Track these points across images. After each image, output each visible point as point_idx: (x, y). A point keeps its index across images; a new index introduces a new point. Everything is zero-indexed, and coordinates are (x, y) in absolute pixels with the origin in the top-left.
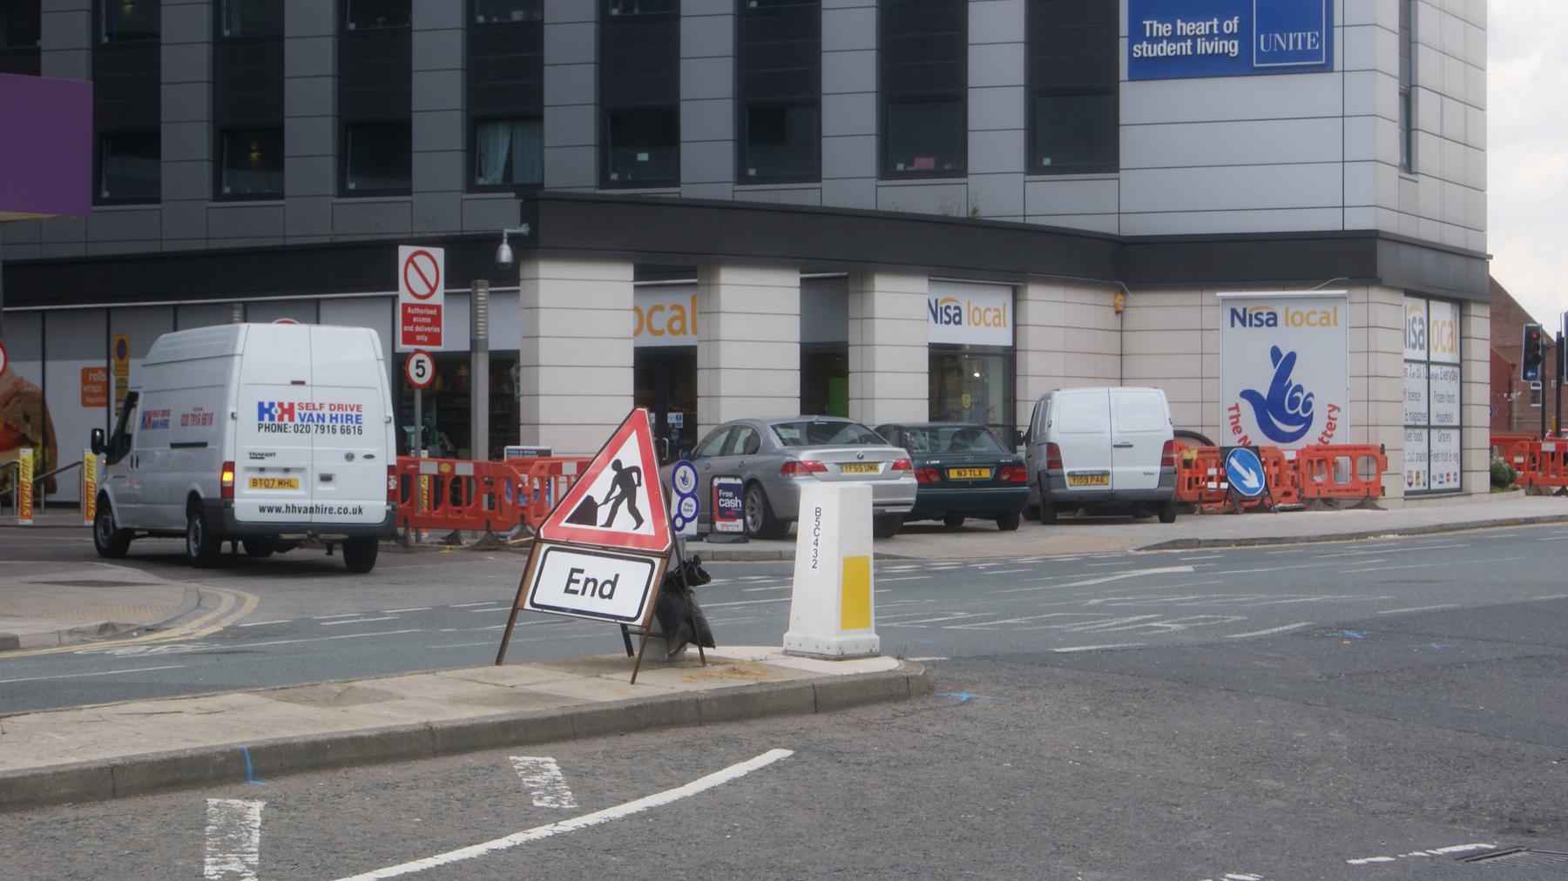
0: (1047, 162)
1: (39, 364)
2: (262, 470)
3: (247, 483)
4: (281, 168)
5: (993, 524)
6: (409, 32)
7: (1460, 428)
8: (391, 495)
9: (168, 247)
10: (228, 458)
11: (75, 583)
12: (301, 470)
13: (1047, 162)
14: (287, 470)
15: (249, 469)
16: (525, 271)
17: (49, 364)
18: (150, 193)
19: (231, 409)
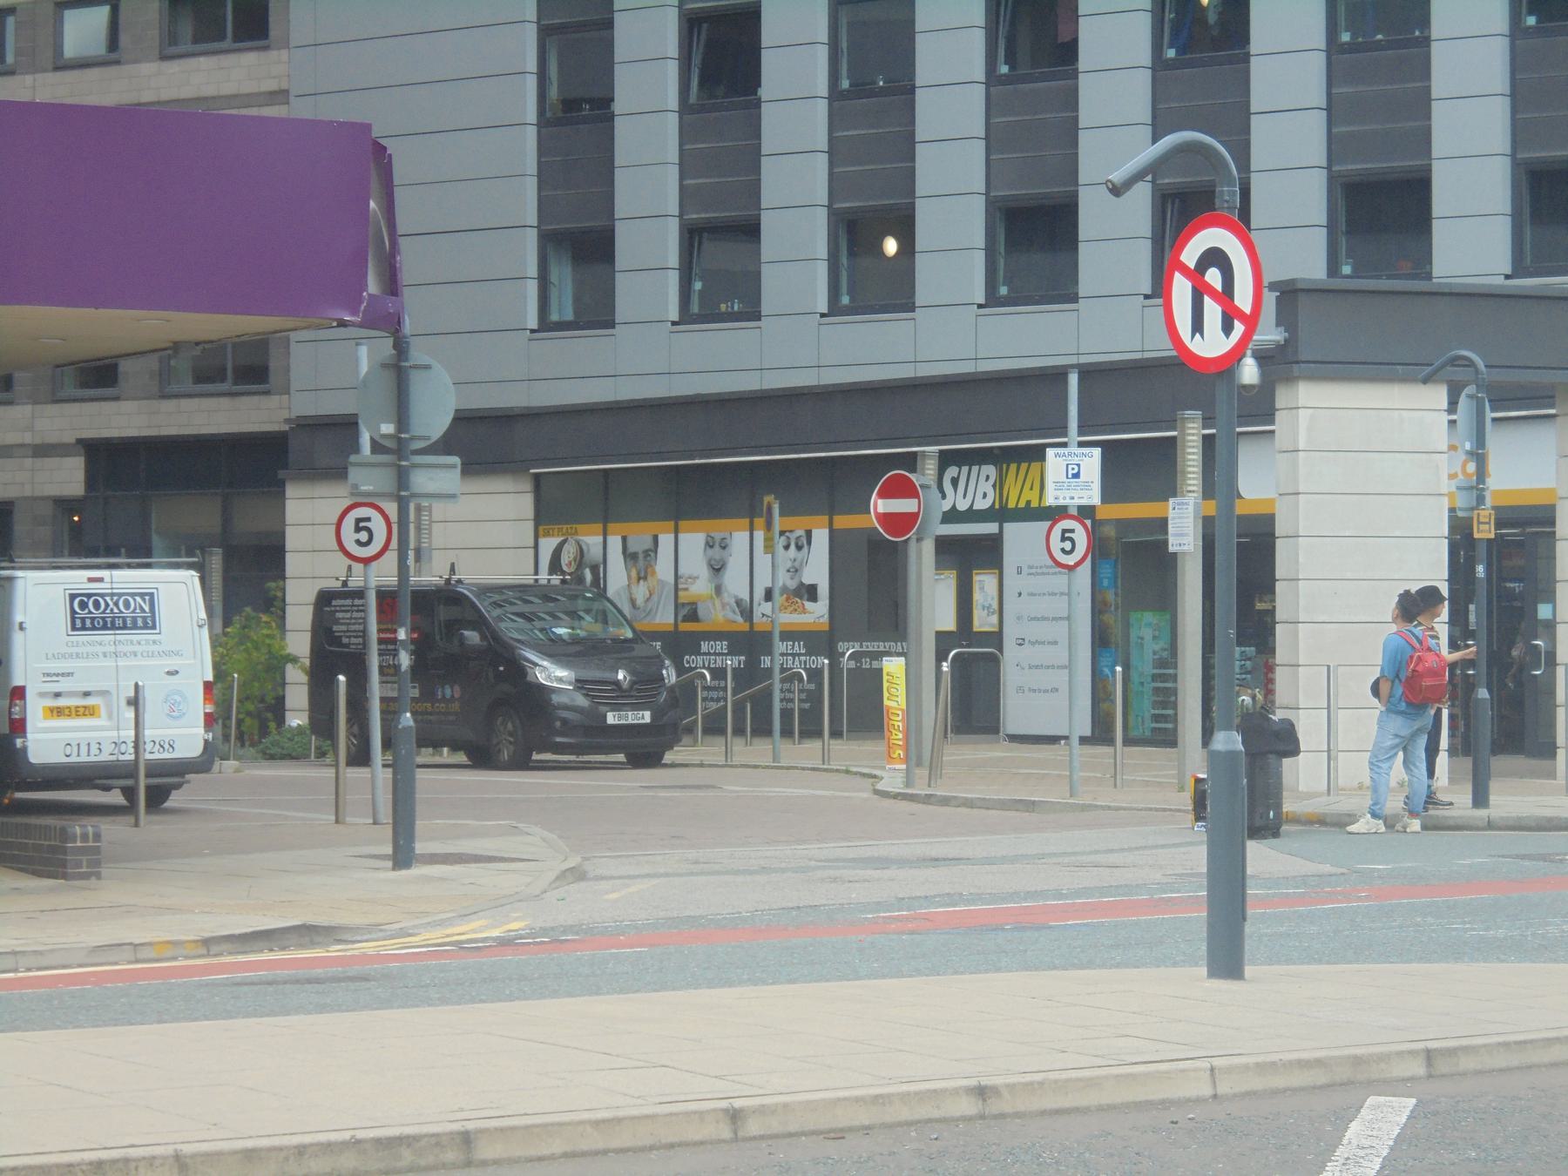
0: (891, 246)
1: (672, 536)
2: (57, 695)
3: (40, 713)
4: (1076, 249)
5: (461, 758)
6: (1426, 42)
7: (1068, 618)
8: (209, 720)
9: (925, 371)
10: (18, 681)
11: (1004, 805)
12: (104, 693)
13: (891, 246)
14: (87, 694)
15: (42, 695)
16: (1282, 397)
17: (681, 536)
18: (1059, 287)
19: (18, 618)
